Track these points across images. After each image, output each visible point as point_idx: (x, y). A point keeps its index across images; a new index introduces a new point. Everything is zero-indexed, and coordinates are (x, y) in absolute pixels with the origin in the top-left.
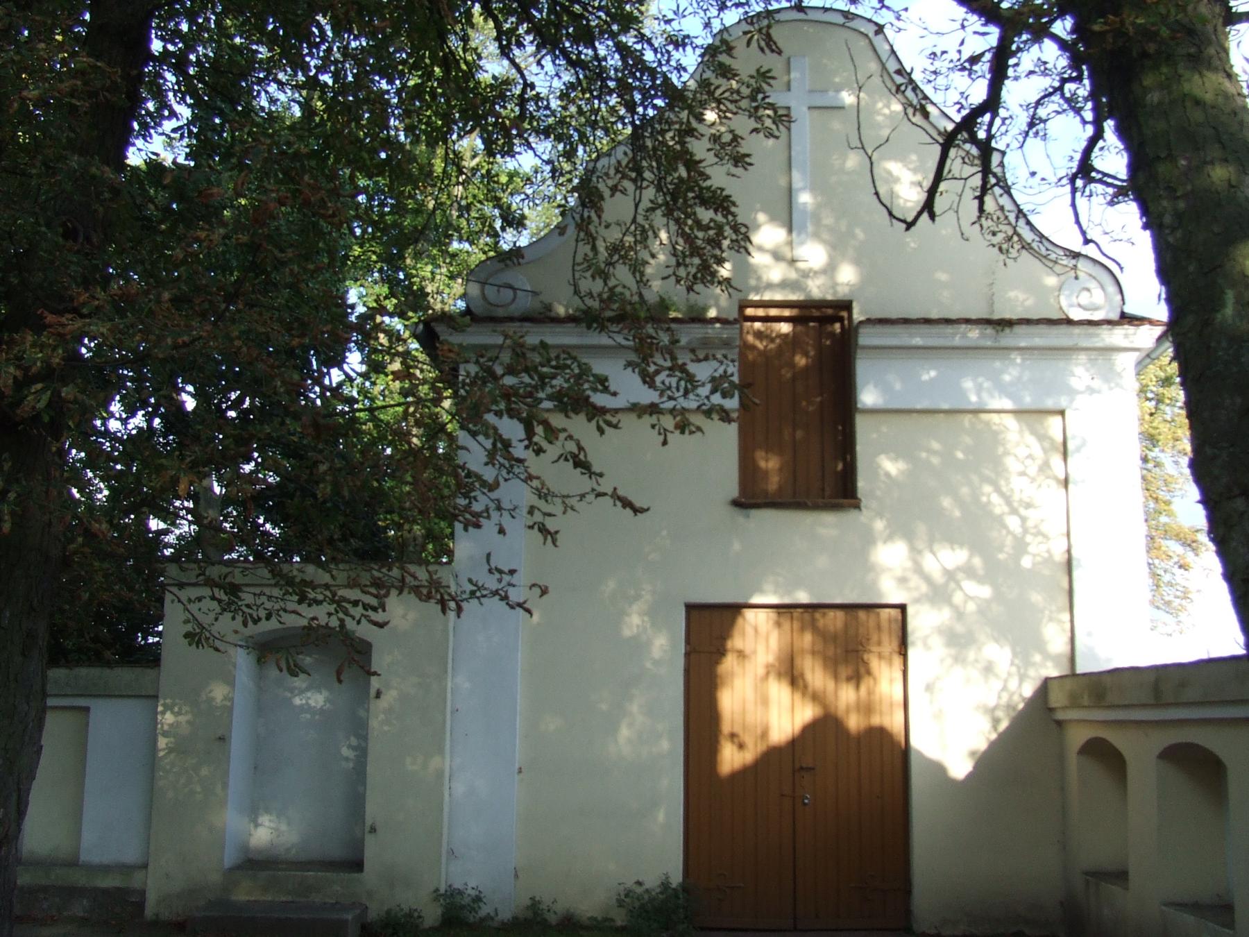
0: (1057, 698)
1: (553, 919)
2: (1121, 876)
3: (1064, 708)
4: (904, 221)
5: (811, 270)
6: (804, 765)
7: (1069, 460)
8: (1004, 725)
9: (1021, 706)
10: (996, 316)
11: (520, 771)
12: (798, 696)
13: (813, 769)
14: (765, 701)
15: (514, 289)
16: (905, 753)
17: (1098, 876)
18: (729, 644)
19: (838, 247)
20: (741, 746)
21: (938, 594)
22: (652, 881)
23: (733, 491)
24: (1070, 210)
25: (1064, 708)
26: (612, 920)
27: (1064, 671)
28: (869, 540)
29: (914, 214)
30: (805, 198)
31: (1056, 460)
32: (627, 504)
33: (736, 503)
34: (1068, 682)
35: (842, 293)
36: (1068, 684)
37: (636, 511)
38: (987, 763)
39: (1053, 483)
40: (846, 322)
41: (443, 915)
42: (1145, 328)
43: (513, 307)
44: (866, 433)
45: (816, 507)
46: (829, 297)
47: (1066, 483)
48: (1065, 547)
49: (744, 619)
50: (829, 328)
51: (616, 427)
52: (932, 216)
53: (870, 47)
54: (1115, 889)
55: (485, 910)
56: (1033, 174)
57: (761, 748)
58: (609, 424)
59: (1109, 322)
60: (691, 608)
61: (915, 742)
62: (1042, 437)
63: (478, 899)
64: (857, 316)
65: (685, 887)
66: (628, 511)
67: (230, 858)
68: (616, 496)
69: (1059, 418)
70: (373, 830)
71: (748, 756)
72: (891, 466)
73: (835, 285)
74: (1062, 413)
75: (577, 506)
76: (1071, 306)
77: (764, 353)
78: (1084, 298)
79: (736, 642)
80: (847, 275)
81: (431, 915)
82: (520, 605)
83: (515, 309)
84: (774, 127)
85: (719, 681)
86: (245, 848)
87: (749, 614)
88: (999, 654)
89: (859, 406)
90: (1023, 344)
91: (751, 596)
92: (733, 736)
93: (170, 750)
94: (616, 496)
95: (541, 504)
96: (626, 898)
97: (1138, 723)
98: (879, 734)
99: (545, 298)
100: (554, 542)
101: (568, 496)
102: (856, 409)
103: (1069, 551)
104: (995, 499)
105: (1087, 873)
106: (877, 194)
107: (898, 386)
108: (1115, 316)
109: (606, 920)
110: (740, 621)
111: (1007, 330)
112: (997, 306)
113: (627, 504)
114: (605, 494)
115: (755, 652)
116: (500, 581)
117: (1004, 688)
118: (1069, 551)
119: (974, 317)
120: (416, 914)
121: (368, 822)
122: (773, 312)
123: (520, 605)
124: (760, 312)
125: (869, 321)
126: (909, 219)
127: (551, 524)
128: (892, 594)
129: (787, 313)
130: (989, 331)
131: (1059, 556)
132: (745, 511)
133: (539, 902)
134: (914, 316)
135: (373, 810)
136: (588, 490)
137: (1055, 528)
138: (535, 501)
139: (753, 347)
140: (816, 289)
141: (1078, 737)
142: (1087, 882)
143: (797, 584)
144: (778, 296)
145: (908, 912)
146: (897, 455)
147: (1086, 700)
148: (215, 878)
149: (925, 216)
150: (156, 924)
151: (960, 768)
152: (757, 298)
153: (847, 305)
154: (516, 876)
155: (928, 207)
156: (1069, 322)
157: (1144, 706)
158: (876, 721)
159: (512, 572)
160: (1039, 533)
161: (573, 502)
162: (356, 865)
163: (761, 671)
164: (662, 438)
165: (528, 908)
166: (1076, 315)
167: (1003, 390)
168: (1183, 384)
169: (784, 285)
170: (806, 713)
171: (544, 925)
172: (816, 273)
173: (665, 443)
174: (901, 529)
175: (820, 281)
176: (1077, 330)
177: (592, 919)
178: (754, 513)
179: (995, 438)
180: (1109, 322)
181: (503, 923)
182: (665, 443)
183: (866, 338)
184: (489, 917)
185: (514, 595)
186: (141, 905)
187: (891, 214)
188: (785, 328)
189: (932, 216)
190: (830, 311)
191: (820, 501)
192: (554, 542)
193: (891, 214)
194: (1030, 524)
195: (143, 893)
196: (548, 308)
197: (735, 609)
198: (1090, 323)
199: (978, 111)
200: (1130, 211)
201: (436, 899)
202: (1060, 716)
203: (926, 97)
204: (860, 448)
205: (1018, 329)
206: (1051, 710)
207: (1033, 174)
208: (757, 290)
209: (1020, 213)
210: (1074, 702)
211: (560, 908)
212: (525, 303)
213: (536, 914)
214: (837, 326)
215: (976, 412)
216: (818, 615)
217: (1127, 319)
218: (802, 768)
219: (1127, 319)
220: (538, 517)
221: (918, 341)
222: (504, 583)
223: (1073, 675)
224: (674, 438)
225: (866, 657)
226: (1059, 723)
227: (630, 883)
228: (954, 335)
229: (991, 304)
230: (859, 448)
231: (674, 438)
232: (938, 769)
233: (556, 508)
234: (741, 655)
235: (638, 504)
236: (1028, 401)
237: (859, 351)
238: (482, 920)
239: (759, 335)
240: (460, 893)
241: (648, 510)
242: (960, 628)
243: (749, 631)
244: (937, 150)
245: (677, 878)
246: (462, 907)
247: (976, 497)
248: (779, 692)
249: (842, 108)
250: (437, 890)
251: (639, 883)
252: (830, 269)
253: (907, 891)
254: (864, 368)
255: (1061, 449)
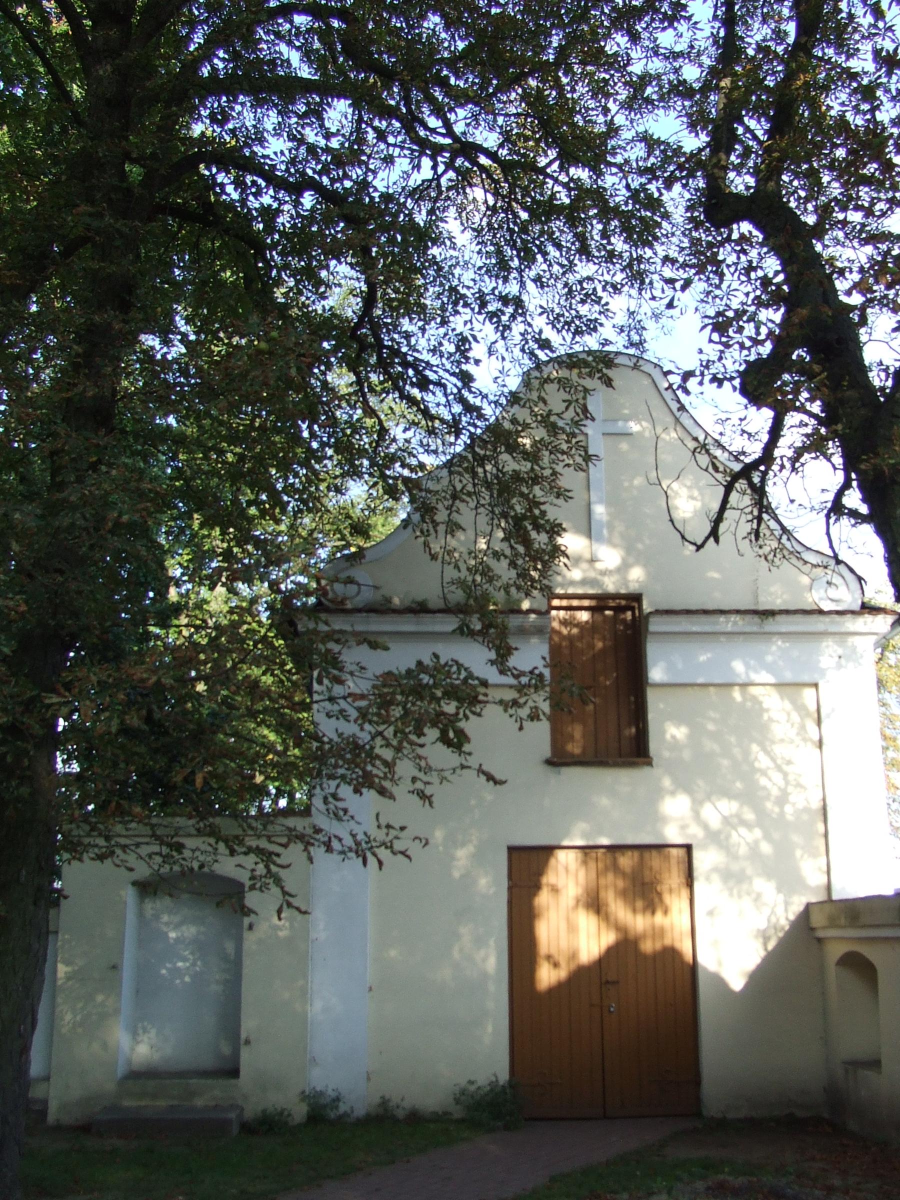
0: (817, 920)
1: (400, 1114)
2: (875, 1064)
3: (824, 928)
4: (695, 544)
5: (607, 570)
6: (610, 979)
7: (823, 726)
8: (771, 946)
9: (787, 928)
10: (761, 607)
11: (370, 989)
12: (603, 925)
13: (618, 982)
14: (572, 928)
15: (359, 585)
16: (694, 967)
17: (855, 1065)
18: (544, 880)
19: (632, 555)
20: (556, 965)
21: (715, 837)
22: (483, 1079)
23: (547, 752)
24: (826, 537)
25: (824, 928)
26: (451, 1114)
27: (822, 897)
28: (657, 794)
29: (703, 539)
30: (599, 510)
31: (811, 726)
32: (490, 778)
33: (549, 762)
34: (827, 906)
35: (633, 588)
36: (827, 907)
37: (496, 782)
38: (757, 978)
39: (809, 744)
40: (637, 612)
41: (308, 1112)
42: (880, 617)
43: (358, 598)
44: (655, 703)
45: (616, 765)
46: (623, 591)
47: (820, 744)
48: (821, 797)
49: (557, 861)
50: (622, 616)
51: (479, 715)
52: (717, 541)
53: (652, 385)
54: (870, 1074)
55: (343, 1108)
56: (792, 501)
57: (573, 966)
58: (474, 713)
59: (853, 612)
60: (512, 850)
61: (701, 959)
62: (801, 709)
63: (337, 1099)
64: (647, 607)
65: (512, 1084)
66: (491, 783)
67: (121, 1071)
68: (481, 771)
69: (813, 690)
70: (247, 1042)
71: (562, 974)
72: (676, 732)
73: (626, 582)
74: (816, 685)
75: (450, 778)
76: (821, 599)
77: (570, 638)
78: (832, 593)
79: (549, 878)
80: (636, 576)
81: (300, 1112)
82: (403, 853)
83: (359, 602)
84: (584, 463)
85: (536, 912)
86: (129, 1062)
87: (561, 855)
88: (765, 887)
89: (650, 681)
90: (783, 630)
91: (562, 840)
92: (549, 957)
93: (69, 978)
94: (481, 771)
95: (421, 775)
96: (461, 1096)
97: (887, 939)
98: (671, 954)
99: (385, 591)
100: (431, 804)
101: (442, 770)
102: (647, 683)
103: (824, 800)
104: (761, 756)
105: (844, 1063)
106: (671, 521)
107: (680, 666)
108: (857, 606)
109: (446, 1113)
110: (552, 861)
111: (771, 619)
112: (762, 599)
113: (490, 778)
114: (469, 767)
115: (566, 886)
116: (387, 834)
117: (773, 912)
118: (824, 800)
119: (743, 608)
120: (286, 1113)
121: (243, 1036)
122: (575, 603)
123: (403, 853)
124: (564, 603)
125: (658, 612)
126: (699, 543)
127: (428, 792)
128: (673, 835)
129: (586, 603)
130: (756, 619)
131: (816, 804)
132: (557, 769)
133: (389, 1100)
134: (694, 608)
135: (248, 1025)
136: (458, 764)
137: (812, 781)
138: (416, 773)
139: (559, 633)
140: (610, 585)
141: (836, 951)
142: (847, 1071)
143: (601, 833)
144: (580, 591)
145: (698, 1100)
146: (679, 721)
147: (843, 921)
148: (110, 1087)
149: (712, 539)
150: (58, 1129)
151: (737, 983)
152: (562, 592)
153: (636, 598)
154: (369, 1079)
155: (714, 534)
156: (821, 612)
157: (892, 926)
158: (667, 942)
159: (402, 829)
160: (799, 785)
161: (447, 774)
162: (234, 1072)
163: (572, 903)
164: (519, 724)
165: (379, 1105)
166: (826, 606)
167: (770, 669)
168: (836, 291)
169: (584, 582)
170: (609, 938)
171: (395, 1120)
172: (611, 572)
173: (521, 728)
174: (684, 785)
175: (614, 578)
176: (827, 619)
177: (435, 1113)
178: (565, 770)
179: (758, 708)
180: (853, 612)
181: (358, 1119)
182: (521, 728)
183: (655, 625)
184: (346, 1114)
185: (398, 846)
186: (44, 1113)
187: (683, 537)
188: (584, 616)
189: (717, 541)
190: (623, 602)
191: (619, 760)
192: (431, 804)
193: (683, 537)
194: (791, 778)
195: (45, 1102)
196: (389, 600)
197: (548, 851)
198: (838, 613)
199: (755, 465)
200: (867, 531)
201: (303, 1100)
202: (820, 934)
203: (716, 458)
204: (651, 716)
205: (778, 618)
206: (813, 929)
207: (792, 501)
208: (562, 586)
209: (784, 529)
210: (833, 923)
211: (407, 1104)
212: (367, 596)
213: (386, 1110)
214: (629, 615)
215: (744, 685)
216: (618, 855)
217: (868, 609)
218: (607, 982)
219: (868, 609)
220: (419, 785)
221: (695, 629)
222: (390, 837)
223: (830, 900)
224: (527, 724)
225: (659, 889)
226: (820, 940)
227: (463, 1082)
228: (727, 622)
229: (756, 597)
230: (650, 716)
231: (527, 724)
232: (719, 982)
233: (434, 778)
234: (555, 890)
235: (498, 776)
236: (789, 677)
237: (649, 638)
238: (340, 1117)
239: (564, 623)
240: (321, 1094)
241: (505, 782)
242: (735, 867)
243: (561, 869)
244: (721, 490)
245: (504, 1076)
246: (325, 1106)
247: (746, 753)
248: (586, 921)
249: (631, 434)
250: (303, 1092)
251: (471, 1082)
252: (623, 568)
253: (697, 1080)
254: (653, 650)
255: (816, 715)
